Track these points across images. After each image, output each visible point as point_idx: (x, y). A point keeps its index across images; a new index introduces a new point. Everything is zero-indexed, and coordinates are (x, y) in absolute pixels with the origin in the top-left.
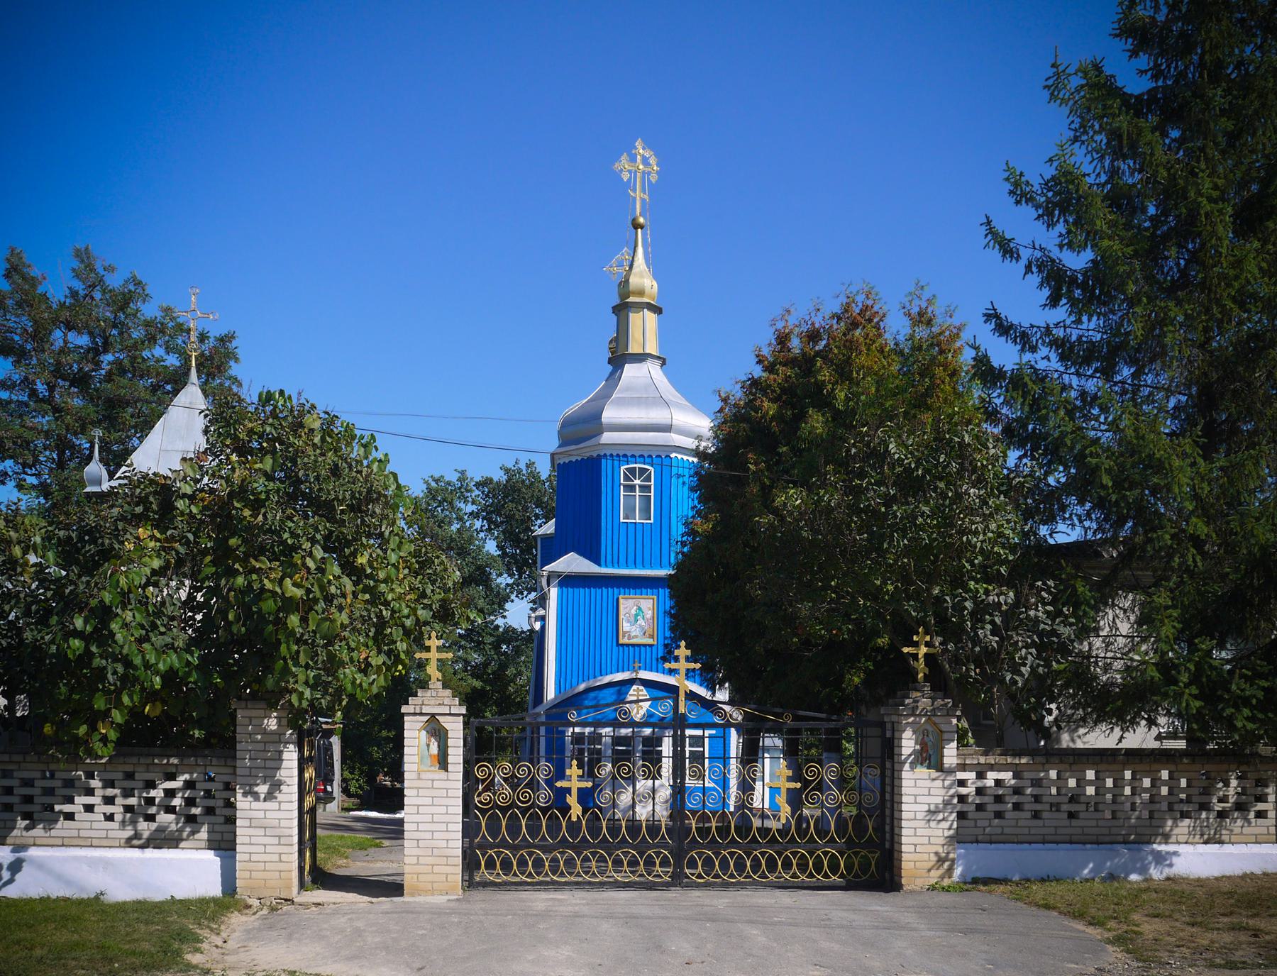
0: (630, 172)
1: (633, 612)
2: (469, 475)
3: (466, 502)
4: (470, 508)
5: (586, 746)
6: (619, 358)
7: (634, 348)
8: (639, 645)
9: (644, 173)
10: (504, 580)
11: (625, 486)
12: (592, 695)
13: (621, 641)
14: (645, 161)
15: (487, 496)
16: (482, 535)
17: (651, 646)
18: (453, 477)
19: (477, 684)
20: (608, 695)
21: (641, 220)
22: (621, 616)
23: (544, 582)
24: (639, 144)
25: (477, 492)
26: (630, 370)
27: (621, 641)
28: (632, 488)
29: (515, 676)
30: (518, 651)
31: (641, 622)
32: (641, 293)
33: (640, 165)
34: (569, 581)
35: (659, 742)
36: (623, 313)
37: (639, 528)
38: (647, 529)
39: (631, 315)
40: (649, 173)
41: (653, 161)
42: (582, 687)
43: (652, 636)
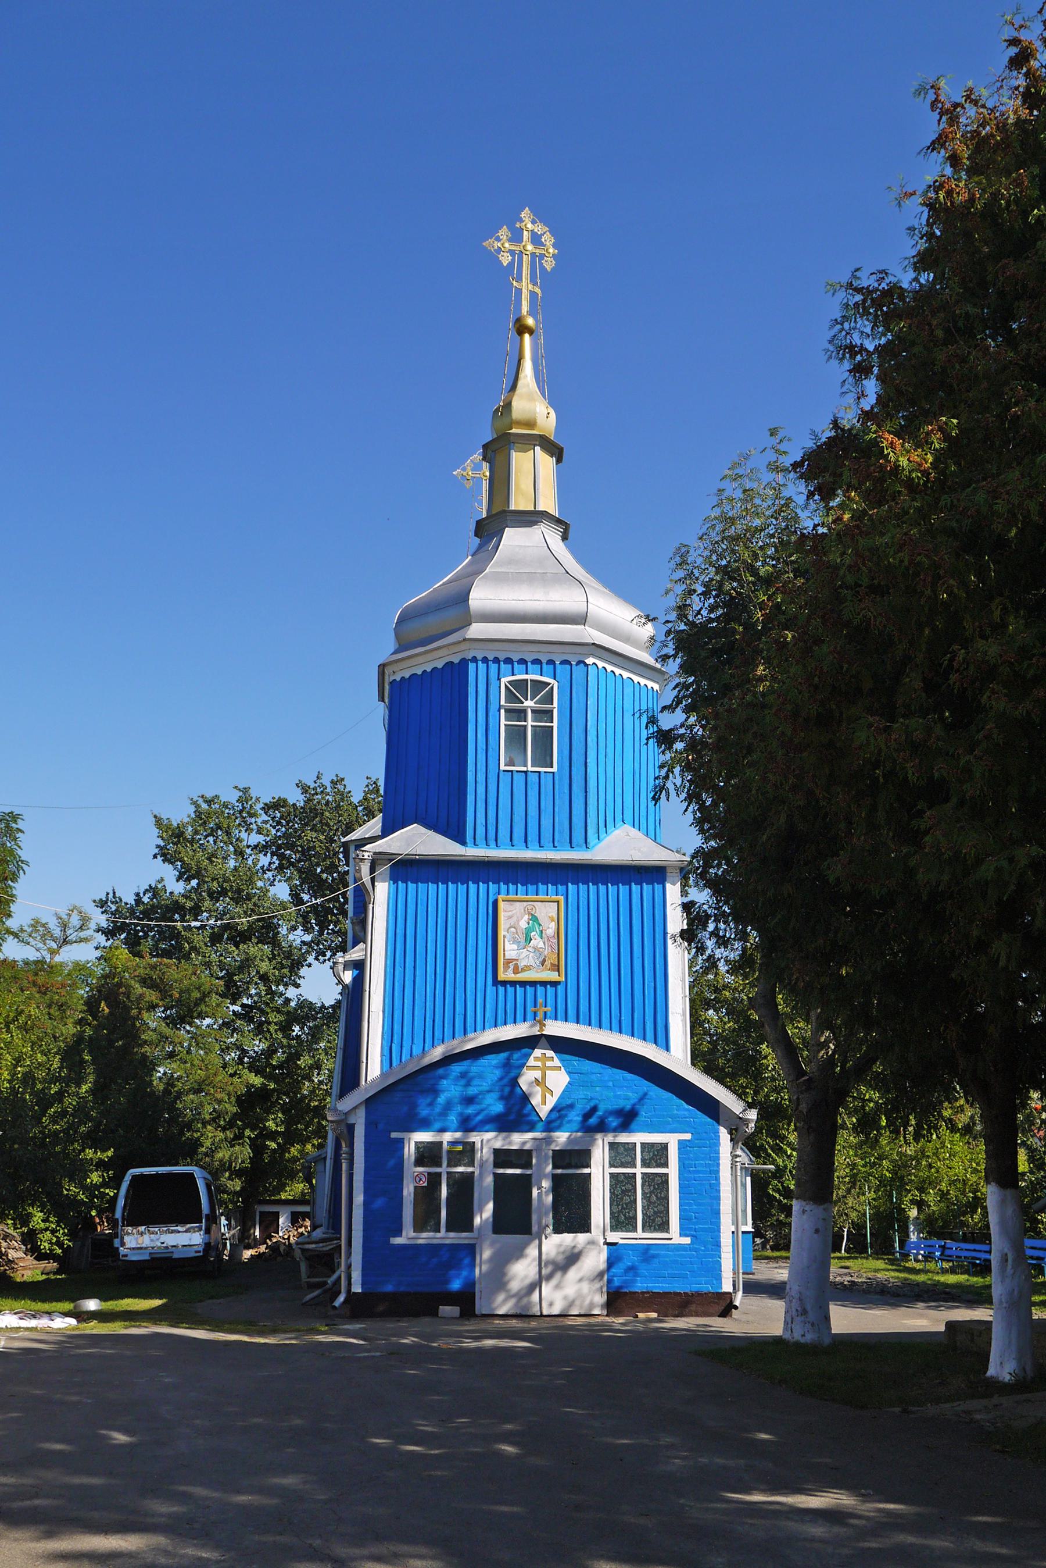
0: (512, 252)
1: (523, 924)
2: (254, 793)
3: (248, 830)
4: (255, 839)
5: (443, 1169)
6: (489, 530)
7: (519, 502)
8: (533, 984)
9: (533, 254)
10: (298, 937)
11: (507, 711)
12: (457, 1069)
13: (502, 976)
14: (536, 239)
15: (279, 823)
16: (269, 874)
17: (555, 984)
18: (232, 797)
19: (257, 1080)
20: (490, 1068)
21: (530, 321)
22: (502, 932)
23: (365, 868)
24: (526, 214)
25: (265, 817)
26: (512, 538)
27: (502, 976)
28: (521, 714)
29: (311, 1067)
30: (315, 1035)
31: (537, 942)
32: (531, 424)
33: (526, 246)
34: (407, 869)
35: (583, 1157)
36: (499, 458)
37: (533, 779)
38: (547, 781)
39: (514, 455)
40: (542, 256)
41: (548, 239)
42: (437, 1053)
43: (557, 968)
